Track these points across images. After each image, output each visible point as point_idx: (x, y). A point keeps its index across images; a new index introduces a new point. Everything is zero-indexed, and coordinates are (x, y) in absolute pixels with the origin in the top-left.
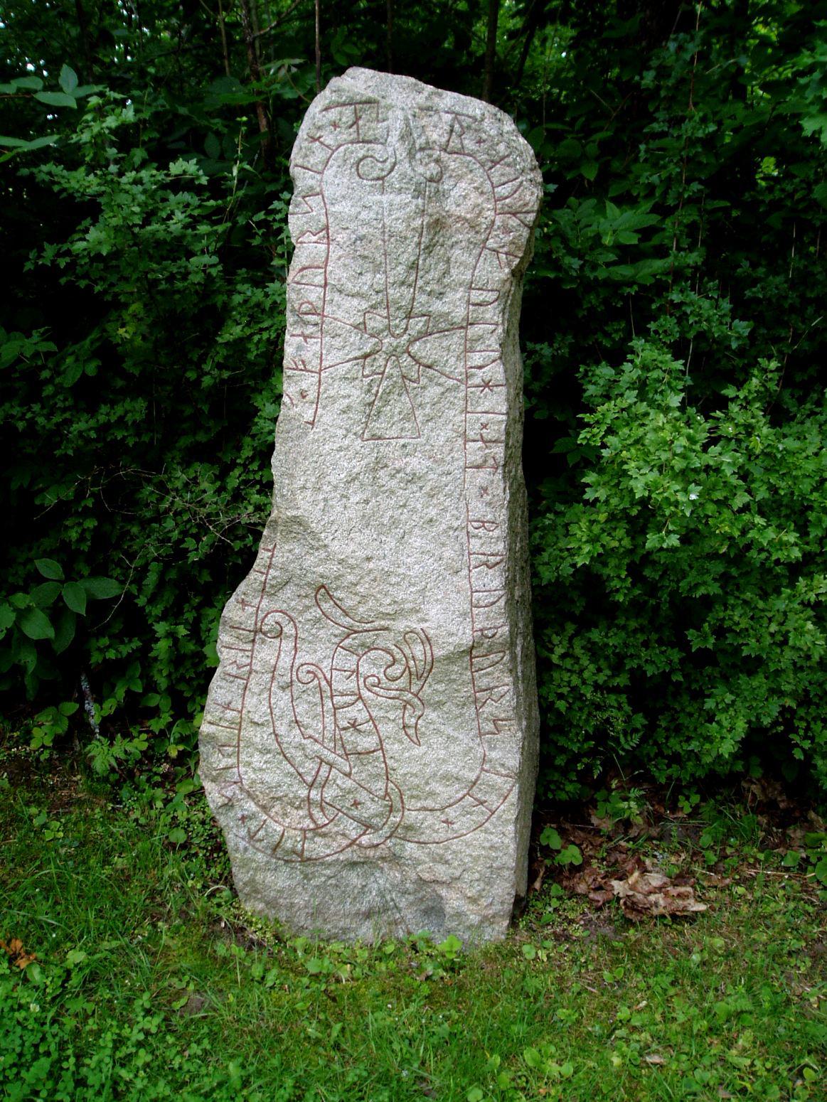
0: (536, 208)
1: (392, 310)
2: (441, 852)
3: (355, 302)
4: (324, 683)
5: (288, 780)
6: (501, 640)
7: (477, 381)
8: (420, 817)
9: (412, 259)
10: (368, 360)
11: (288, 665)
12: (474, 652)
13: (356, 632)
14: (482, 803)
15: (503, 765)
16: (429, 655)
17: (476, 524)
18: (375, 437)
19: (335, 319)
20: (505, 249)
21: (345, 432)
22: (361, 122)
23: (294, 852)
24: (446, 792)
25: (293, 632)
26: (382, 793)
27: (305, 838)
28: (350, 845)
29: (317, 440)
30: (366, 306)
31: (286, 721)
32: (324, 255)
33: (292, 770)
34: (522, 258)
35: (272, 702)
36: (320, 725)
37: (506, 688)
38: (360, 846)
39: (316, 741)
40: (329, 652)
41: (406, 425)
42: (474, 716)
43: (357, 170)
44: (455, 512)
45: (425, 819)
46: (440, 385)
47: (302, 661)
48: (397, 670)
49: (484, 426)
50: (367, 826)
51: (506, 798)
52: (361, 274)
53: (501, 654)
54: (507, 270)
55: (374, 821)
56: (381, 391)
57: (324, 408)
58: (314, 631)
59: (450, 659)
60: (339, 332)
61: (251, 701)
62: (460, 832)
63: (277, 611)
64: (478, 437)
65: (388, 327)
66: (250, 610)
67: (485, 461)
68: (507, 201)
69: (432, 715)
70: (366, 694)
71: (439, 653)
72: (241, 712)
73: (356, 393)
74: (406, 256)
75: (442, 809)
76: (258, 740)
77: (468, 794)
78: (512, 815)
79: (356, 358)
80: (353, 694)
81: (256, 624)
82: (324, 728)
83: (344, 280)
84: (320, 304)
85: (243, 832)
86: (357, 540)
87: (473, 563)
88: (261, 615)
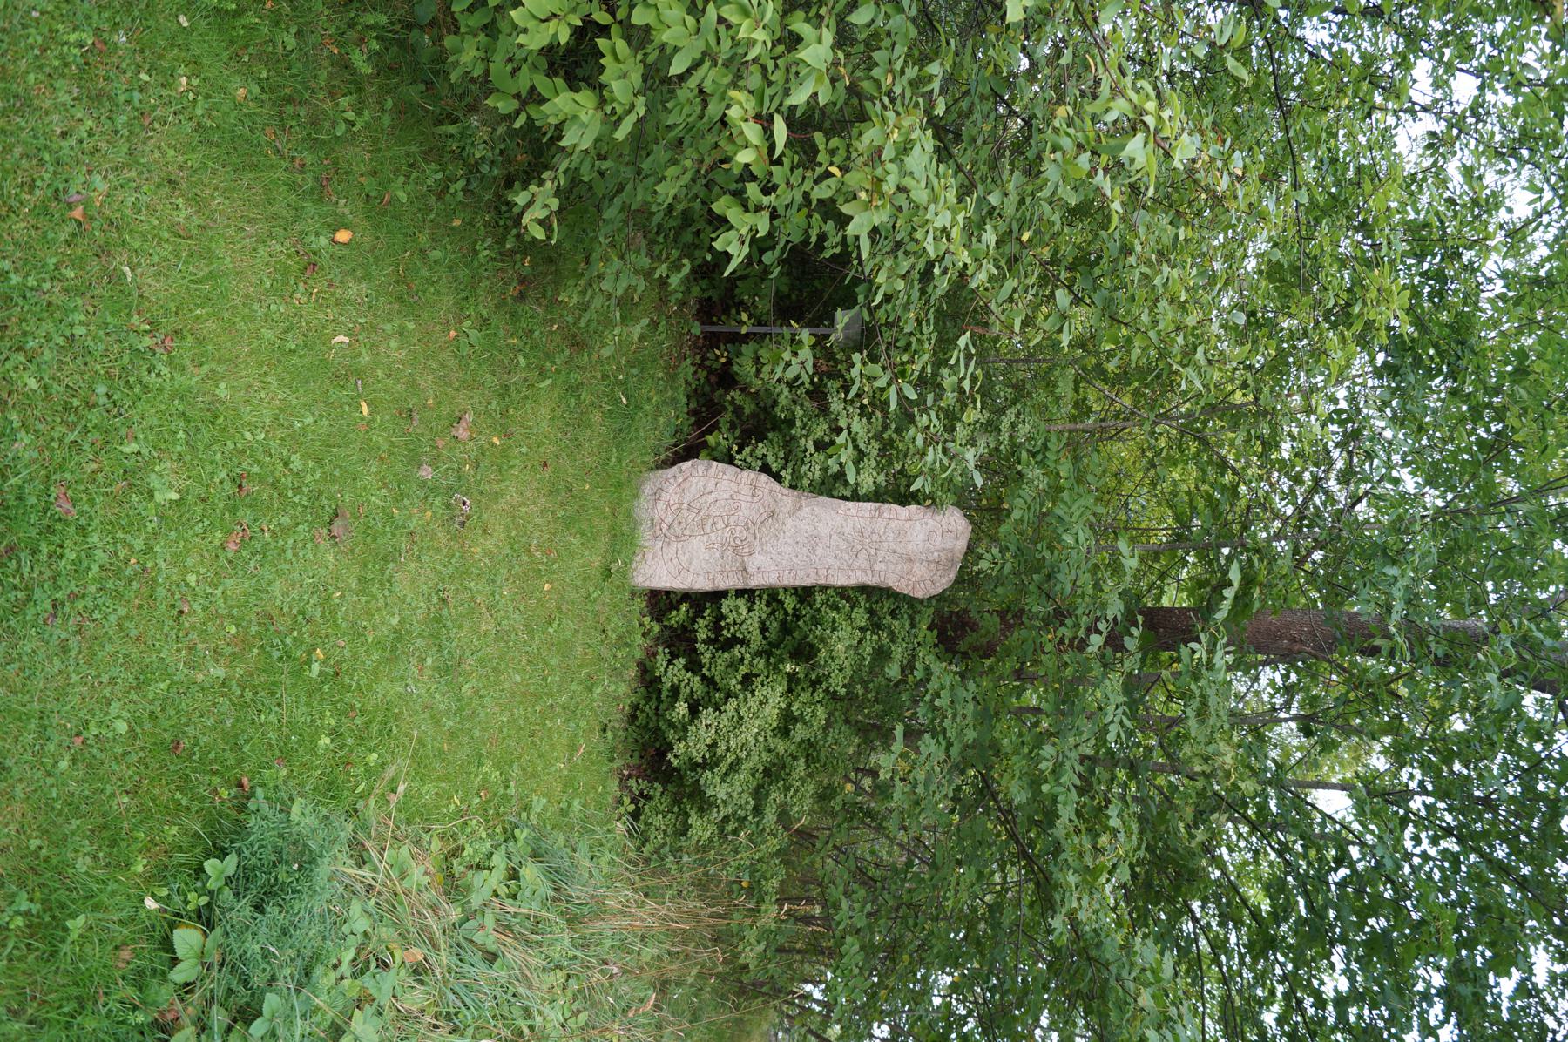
24: (684, 559)
50: (669, 527)
59: (743, 562)
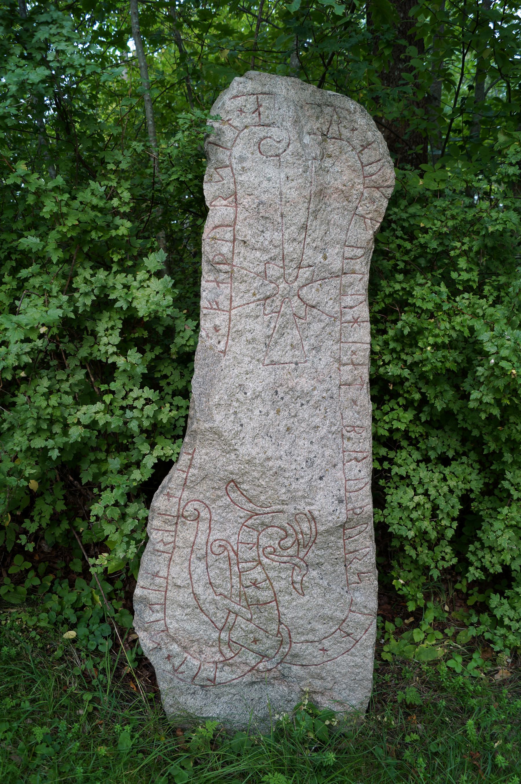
3: (258, 254)
4: (232, 554)
7: (349, 317)
8: (304, 647)
9: (303, 220)
11: (204, 541)
13: (257, 514)
14: (348, 635)
17: (348, 429)
18: (273, 363)
19: (243, 268)
21: (250, 359)
22: (261, 109)
25: (208, 516)
26: (275, 632)
27: (217, 668)
30: (267, 257)
31: (202, 583)
32: (233, 216)
33: (207, 619)
35: (192, 569)
36: (229, 585)
37: (367, 550)
38: (258, 671)
39: (225, 597)
41: (296, 353)
42: (344, 571)
43: (259, 148)
47: (215, 537)
48: (289, 541)
49: (354, 353)
52: (263, 232)
53: (365, 526)
54: (371, 232)
56: (277, 326)
57: (233, 340)
58: (224, 514)
61: (175, 570)
63: (195, 500)
65: (283, 275)
66: (175, 500)
68: (373, 177)
69: (314, 573)
70: (265, 560)
72: (167, 578)
73: (258, 327)
76: (181, 599)
79: (259, 300)
80: (254, 560)
81: (178, 511)
82: (232, 586)
83: (248, 237)
84: (230, 255)
85: (169, 667)
88: (183, 504)
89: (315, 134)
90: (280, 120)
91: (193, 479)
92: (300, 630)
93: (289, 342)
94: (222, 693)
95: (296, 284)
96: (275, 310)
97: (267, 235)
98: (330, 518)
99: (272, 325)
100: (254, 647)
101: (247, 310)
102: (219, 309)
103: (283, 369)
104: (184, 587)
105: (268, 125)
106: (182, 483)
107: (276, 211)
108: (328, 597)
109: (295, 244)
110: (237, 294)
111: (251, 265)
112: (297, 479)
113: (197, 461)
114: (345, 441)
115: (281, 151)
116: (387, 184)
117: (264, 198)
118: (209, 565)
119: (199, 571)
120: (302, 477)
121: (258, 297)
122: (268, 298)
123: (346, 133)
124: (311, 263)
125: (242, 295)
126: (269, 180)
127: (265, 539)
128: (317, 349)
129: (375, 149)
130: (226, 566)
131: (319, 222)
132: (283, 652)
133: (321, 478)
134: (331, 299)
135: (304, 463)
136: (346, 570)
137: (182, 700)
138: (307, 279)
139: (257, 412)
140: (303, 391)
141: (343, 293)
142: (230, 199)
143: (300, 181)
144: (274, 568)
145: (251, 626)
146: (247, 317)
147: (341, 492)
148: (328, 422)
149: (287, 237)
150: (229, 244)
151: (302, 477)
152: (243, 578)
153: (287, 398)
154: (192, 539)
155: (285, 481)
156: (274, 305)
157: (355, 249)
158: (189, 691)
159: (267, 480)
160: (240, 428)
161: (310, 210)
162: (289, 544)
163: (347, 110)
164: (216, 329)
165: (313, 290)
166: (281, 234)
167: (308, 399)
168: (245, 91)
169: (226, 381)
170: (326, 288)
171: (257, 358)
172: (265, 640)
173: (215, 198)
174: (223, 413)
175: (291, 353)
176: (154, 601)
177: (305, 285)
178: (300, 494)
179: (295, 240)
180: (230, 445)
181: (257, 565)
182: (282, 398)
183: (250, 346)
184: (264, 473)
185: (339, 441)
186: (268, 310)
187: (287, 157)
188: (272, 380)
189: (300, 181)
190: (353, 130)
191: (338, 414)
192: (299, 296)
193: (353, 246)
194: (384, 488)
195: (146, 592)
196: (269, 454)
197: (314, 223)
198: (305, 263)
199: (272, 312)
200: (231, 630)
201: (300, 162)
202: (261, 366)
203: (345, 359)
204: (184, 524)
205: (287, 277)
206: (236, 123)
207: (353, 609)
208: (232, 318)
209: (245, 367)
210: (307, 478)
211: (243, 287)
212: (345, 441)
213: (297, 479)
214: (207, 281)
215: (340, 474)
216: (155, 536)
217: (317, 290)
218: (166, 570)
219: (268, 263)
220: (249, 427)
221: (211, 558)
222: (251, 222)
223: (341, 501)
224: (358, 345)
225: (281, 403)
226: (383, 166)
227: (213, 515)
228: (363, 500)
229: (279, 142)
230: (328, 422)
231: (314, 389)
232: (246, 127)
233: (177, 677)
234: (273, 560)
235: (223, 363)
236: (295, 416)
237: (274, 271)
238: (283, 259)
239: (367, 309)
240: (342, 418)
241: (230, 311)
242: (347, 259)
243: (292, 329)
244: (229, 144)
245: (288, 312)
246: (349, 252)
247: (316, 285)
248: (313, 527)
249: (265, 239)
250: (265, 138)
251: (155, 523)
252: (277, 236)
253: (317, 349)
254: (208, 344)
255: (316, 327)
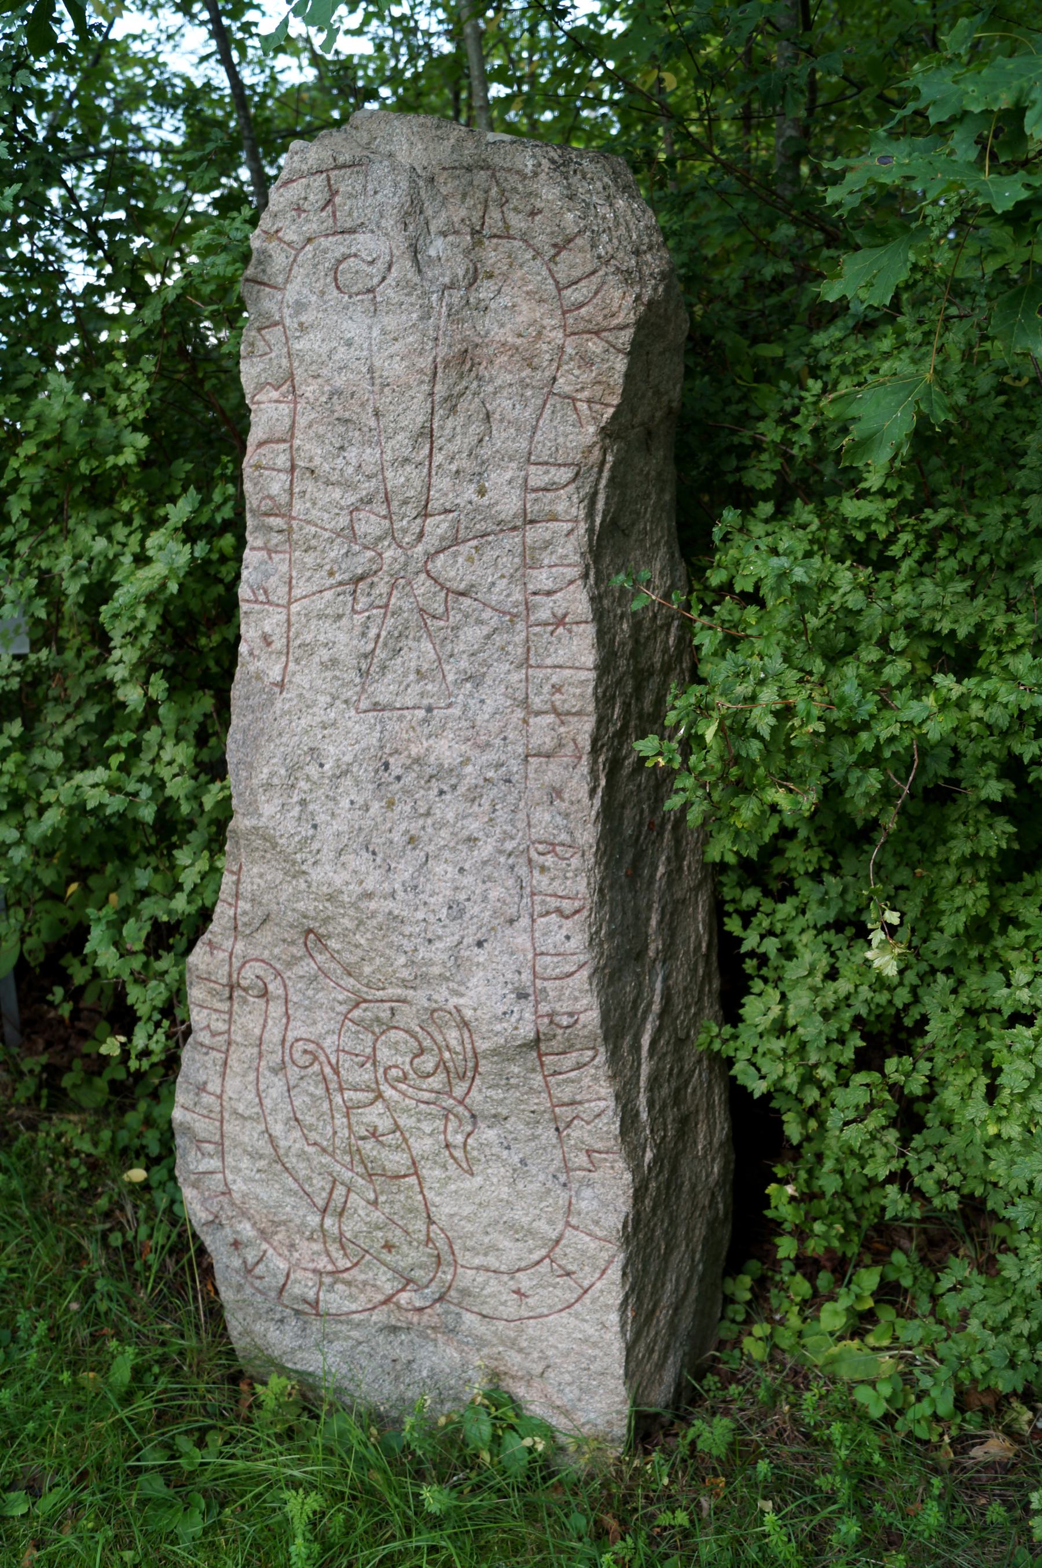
0: (632, 318)
1: (395, 504)
2: (512, 1334)
3: (337, 493)
4: (328, 1070)
5: (291, 1200)
6: (586, 1032)
7: (544, 614)
8: (479, 1279)
9: (420, 419)
10: (361, 585)
11: (277, 1038)
12: (543, 1047)
13: (365, 1001)
14: (568, 1274)
15: (597, 1223)
16: (469, 1047)
17: (541, 848)
18: (376, 707)
19: (309, 522)
20: (586, 394)
21: (329, 699)
22: (338, 200)
23: (305, 1301)
24: (512, 1252)
25: (281, 992)
26: (422, 1237)
27: (321, 1284)
28: (385, 1302)
29: (289, 712)
30: (353, 499)
31: (281, 1116)
32: (287, 422)
33: (295, 1186)
34: (618, 406)
35: (262, 1087)
36: (329, 1128)
37: (602, 1104)
38: (398, 1306)
39: (324, 1150)
40: (334, 1026)
41: (429, 687)
42: (554, 1141)
43: (336, 279)
44: (508, 828)
45: (486, 1283)
46: (482, 622)
47: (297, 1034)
48: (428, 1063)
49: (557, 689)
51: (604, 1272)
52: (342, 448)
53: (590, 1053)
54: (592, 429)
55: (417, 1274)
56: (383, 634)
57: (297, 661)
58: (310, 993)
60: (313, 543)
61: (233, 1084)
62: (539, 1311)
63: (257, 960)
64: (545, 707)
65: (391, 533)
66: (222, 955)
67: (560, 745)
68: (583, 311)
69: (491, 1135)
70: (389, 1092)
71: (482, 1046)
72: (220, 1097)
73: (342, 637)
74: (410, 415)
75: (512, 1273)
76: (246, 1139)
77: (548, 1256)
78: (615, 1298)
79: (340, 584)
80: (368, 1089)
81: (230, 976)
82: (335, 1133)
83: (317, 461)
84: (284, 499)
85: (237, 1263)
86: (352, 866)
87: (538, 908)
88: (236, 964)
89: (456, 232)
90: (375, 217)
91: (245, 919)
92: (470, 1243)
93: (413, 665)
94: (335, 1333)
95: (420, 548)
96: (377, 603)
97: (352, 453)
98: (498, 1027)
99: (373, 632)
100: (388, 1258)
101: (318, 604)
102: (269, 602)
103: (400, 719)
104: (250, 1118)
105: (352, 231)
106: (231, 925)
107: (362, 405)
108: (520, 1186)
109: (408, 468)
110: (300, 571)
111: (326, 516)
112: (430, 941)
113: (246, 887)
114: (536, 873)
115: (376, 281)
116: (615, 322)
117: (339, 381)
118: (292, 1083)
119: (274, 1093)
120: (440, 938)
121: (338, 577)
122: (362, 578)
123: (518, 222)
124: (448, 506)
125: (308, 574)
126: (349, 344)
127: (386, 1050)
128: (475, 679)
129: (581, 250)
130: (320, 1091)
131: (461, 419)
132: (442, 1281)
133: (480, 944)
134: (503, 576)
135: (445, 910)
136: (559, 1137)
137: (259, 1327)
138: (442, 539)
139: (345, 803)
140: (441, 765)
141: (529, 559)
142: (284, 388)
143: (411, 339)
144: (406, 1110)
145: (377, 1216)
146: (319, 617)
147: (524, 976)
148: (498, 830)
149: (388, 456)
150: (283, 476)
151: (440, 938)
152: (353, 1120)
153: (409, 779)
154: (257, 1031)
155: (405, 942)
156: (376, 591)
157: (553, 470)
158: (271, 1315)
159: (369, 936)
160: (311, 832)
161: (437, 398)
162: (430, 1066)
163: (518, 172)
164: (267, 641)
165: (460, 560)
166: (378, 450)
167: (454, 781)
168: (305, 167)
169: (284, 740)
170: (489, 555)
171: (343, 697)
172: (405, 1248)
173: (260, 387)
174: (277, 801)
175: (417, 688)
176: (202, 1135)
177: (443, 550)
178: (436, 970)
179: (407, 460)
180: (294, 863)
181: (376, 1099)
182: (398, 778)
183: (329, 674)
184: (361, 923)
185: (523, 871)
186: (363, 602)
187: (388, 292)
188: (375, 742)
189: (411, 339)
190: (533, 214)
191: (522, 815)
192: (428, 573)
193: (546, 463)
194: (751, 977)
195: (189, 1116)
196: (369, 885)
197: (450, 423)
198: (434, 505)
199: (372, 606)
200: (341, 1214)
201: (413, 299)
202: (353, 712)
203: (537, 702)
204: (245, 1002)
205: (398, 535)
206: (290, 235)
207: (574, 1221)
208: (293, 619)
209: (320, 715)
210: (450, 941)
211: (310, 559)
212: (536, 873)
213: (430, 941)
214: (253, 549)
215: (522, 940)
216: (198, 1017)
217: (470, 559)
218: (218, 1081)
219: (357, 509)
220: (329, 831)
221: (293, 1072)
222: (321, 430)
223: (522, 996)
224: (567, 672)
225: (396, 787)
226: (603, 283)
227: (291, 991)
228: (576, 999)
229: (372, 263)
230: (498, 830)
231: (466, 762)
232: (309, 240)
233: (252, 1285)
234: (404, 1094)
235: (278, 705)
236: (428, 814)
237: (370, 525)
238: (387, 500)
239: (584, 597)
240: (529, 825)
241: (288, 606)
242: (535, 490)
243: (418, 640)
244: (280, 279)
245: (406, 606)
246: (538, 477)
247: (466, 549)
248: (467, 1041)
249: (348, 464)
250: (346, 257)
251: (196, 993)
252: (370, 455)
253: (475, 679)
254: (252, 669)
255: (472, 634)
